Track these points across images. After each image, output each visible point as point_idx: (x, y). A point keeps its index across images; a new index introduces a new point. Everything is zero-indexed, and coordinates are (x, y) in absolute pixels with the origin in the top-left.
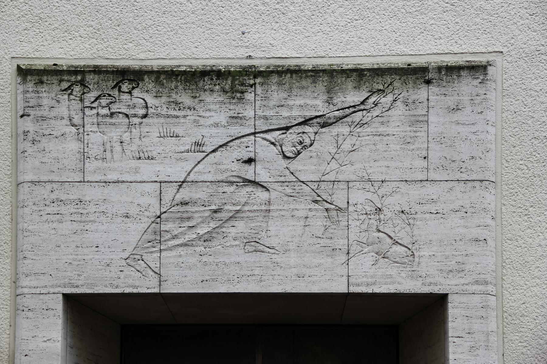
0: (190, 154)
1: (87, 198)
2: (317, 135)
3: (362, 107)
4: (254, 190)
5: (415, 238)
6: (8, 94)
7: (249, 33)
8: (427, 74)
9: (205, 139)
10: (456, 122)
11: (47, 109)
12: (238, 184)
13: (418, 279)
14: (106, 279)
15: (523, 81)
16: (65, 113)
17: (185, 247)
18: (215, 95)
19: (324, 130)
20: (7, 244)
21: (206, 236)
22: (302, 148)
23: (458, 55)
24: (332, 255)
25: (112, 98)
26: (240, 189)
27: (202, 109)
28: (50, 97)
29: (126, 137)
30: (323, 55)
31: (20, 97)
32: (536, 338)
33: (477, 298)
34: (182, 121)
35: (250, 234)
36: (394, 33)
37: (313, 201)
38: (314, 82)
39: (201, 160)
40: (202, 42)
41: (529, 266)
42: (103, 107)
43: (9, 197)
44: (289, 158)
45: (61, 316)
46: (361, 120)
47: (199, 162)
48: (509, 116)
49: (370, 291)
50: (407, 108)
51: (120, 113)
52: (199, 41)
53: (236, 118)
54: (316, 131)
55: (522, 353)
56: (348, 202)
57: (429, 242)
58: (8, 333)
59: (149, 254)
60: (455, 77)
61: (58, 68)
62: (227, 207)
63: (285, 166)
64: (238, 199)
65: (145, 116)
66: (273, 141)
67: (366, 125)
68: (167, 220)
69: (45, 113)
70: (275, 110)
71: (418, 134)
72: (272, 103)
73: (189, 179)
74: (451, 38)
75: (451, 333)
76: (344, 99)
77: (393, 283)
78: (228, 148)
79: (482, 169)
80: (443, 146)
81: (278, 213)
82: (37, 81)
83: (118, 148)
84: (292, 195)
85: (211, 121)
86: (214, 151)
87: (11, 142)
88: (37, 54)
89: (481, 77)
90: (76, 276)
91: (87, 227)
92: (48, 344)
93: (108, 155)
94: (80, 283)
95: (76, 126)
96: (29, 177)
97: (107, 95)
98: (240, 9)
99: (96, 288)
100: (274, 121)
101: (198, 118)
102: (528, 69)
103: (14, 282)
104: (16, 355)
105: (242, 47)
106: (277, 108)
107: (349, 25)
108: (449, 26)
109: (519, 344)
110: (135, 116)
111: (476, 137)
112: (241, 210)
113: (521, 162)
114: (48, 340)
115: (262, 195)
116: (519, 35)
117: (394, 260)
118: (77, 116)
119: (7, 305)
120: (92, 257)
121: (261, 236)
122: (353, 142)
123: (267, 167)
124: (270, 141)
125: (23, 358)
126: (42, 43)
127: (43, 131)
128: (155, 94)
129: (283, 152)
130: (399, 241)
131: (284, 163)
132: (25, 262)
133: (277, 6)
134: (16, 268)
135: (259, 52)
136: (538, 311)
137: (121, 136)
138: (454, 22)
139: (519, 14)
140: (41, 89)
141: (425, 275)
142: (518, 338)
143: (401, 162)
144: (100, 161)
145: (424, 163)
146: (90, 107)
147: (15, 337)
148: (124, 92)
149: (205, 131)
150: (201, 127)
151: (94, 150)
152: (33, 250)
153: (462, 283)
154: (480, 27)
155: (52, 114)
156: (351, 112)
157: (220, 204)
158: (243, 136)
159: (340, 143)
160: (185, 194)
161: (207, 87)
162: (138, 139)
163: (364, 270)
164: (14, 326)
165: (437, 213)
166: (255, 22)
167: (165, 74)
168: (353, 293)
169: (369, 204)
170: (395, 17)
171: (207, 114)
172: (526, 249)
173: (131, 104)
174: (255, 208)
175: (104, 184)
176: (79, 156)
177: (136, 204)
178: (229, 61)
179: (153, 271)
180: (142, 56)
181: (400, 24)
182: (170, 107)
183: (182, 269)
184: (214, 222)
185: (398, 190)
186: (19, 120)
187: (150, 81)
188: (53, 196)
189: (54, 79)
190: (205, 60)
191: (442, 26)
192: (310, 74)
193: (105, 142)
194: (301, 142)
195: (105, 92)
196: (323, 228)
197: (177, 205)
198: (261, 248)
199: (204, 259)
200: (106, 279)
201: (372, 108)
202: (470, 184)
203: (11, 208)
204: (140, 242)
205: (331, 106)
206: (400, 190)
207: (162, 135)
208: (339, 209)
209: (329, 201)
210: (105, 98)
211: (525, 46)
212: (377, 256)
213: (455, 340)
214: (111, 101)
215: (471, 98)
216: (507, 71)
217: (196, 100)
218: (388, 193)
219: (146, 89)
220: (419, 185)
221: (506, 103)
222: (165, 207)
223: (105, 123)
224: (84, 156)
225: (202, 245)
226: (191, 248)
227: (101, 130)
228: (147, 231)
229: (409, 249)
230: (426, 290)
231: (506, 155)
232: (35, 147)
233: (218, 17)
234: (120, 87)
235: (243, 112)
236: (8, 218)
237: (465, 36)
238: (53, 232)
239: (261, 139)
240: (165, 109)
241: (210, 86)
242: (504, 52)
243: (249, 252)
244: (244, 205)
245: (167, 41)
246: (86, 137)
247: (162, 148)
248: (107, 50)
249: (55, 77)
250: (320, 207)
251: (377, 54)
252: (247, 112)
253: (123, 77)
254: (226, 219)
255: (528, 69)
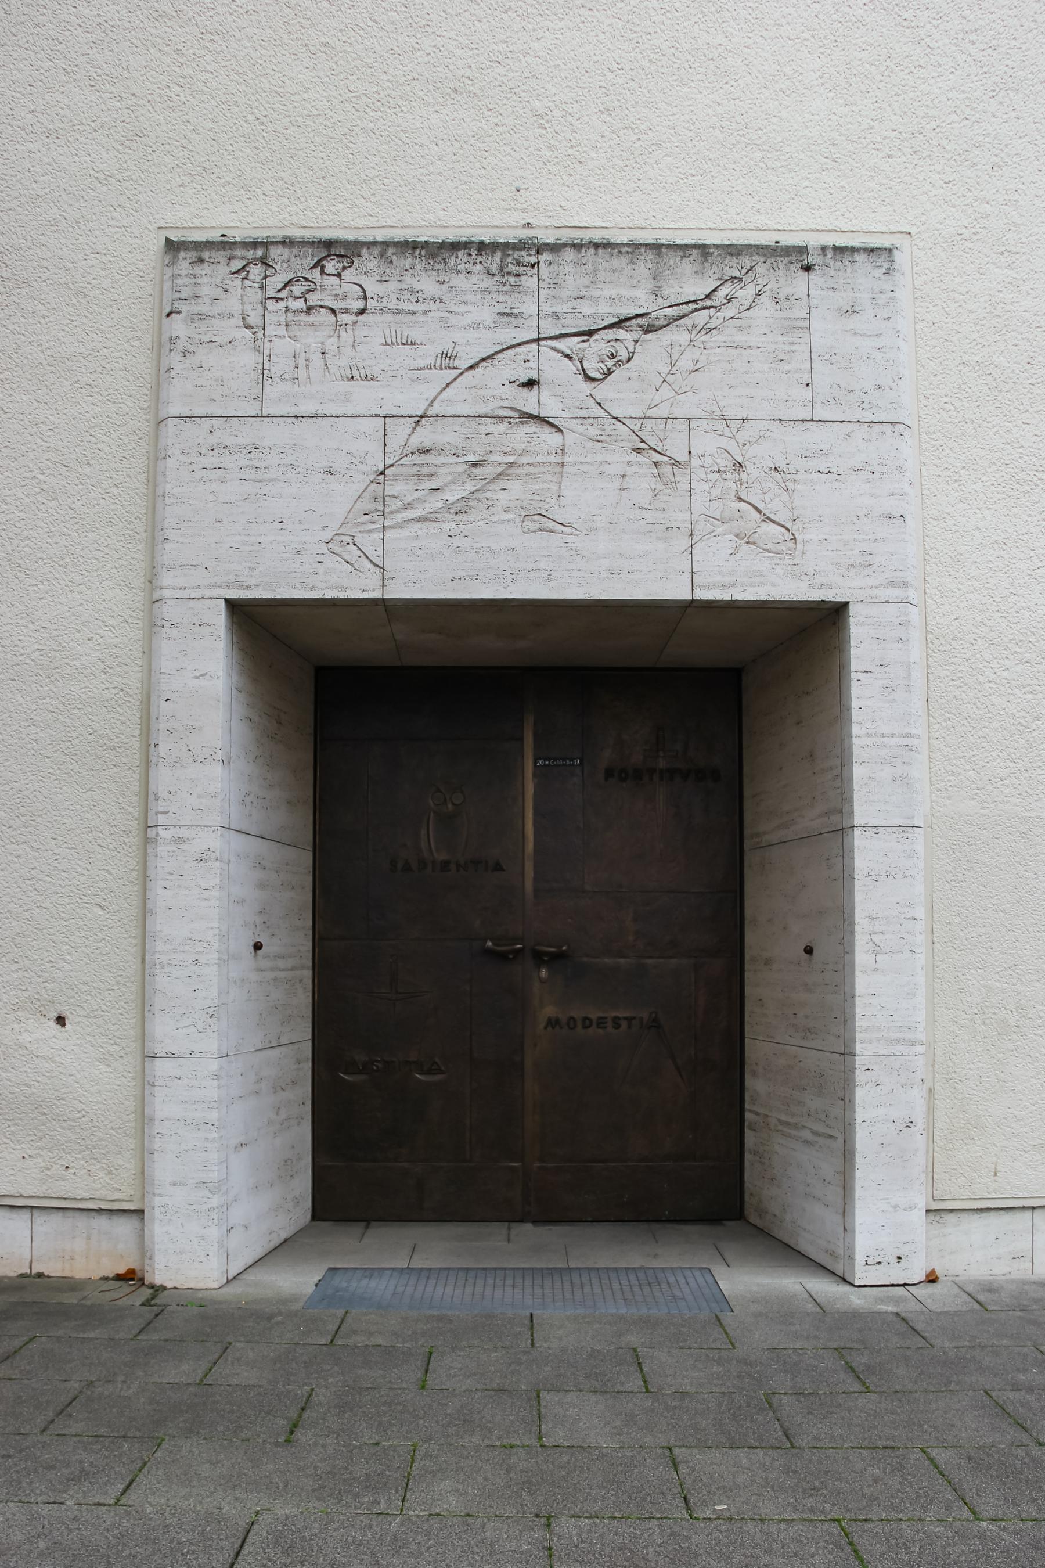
0: (434, 371)
1: (267, 443)
2: (638, 344)
3: (708, 303)
4: (537, 430)
5: (796, 512)
6: (149, 283)
7: (527, 189)
8: (805, 256)
9: (457, 348)
10: (853, 332)
11: (208, 301)
12: (512, 420)
13: (802, 578)
14: (295, 575)
15: (942, 278)
16: (236, 308)
17: (426, 523)
18: (475, 279)
19: (649, 336)
20: (140, 520)
21: (459, 504)
22: (614, 365)
23: (847, 234)
24: (666, 538)
25: (309, 283)
26: (514, 428)
27: (452, 301)
28: (213, 284)
29: (331, 344)
30: (644, 225)
31: (167, 285)
32: (975, 673)
33: (892, 609)
34: (422, 320)
35: (531, 502)
36: (750, 197)
37: (634, 450)
38: (632, 262)
39: (452, 382)
40: (453, 203)
41: (962, 561)
42: (296, 298)
43: (144, 444)
44: (593, 380)
45: (223, 636)
46: (708, 323)
47: (448, 385)
48: (926, 329)
49: (727, 598)
50: (778, 306)
51: (321, 307)
52: (449, 200)
53: (508, 315)
54: (636, 338)
55: (955, 697)
56: (690, 452)
57: (817, 518)
58: (140, 663)
59: (365, 535)
60: (847, 263)
61: (227, 239)
62: (493, 458)
63: (588, 393)
64: (511, 445)
65: (362, 312)
66: (568, 352)
67: (714, 331)
68: (395, 478)
69: (204, 309)
70: (570, 305)
71: (794, 348)
72: (565, 293)
73: (432, 411)
74: (835, 209)
75: (854, 665)
76: (680, 290)
77: (762, 584)
78: (495, 362)
79: (893, 405)
80: (834, 366)
81: (577, 467)
82: (194, 259)
83: (317, 362)
84: (599, 438)
85: (468, 320)
86: (471, 367)
87: (152, 358)
88: (197, 223)
89: (886, 265)
90: (247, 570)
91: (265, 490)
92: (202, 682)
93: (302, 373)
94: (252, 581)
95: (252, 328)
96: (174, 410)
97: (302, 279)
98: (513, 153)
99: (279, 590)
100: (569, 321)
101: (446, 315)
102: (948, 261)
103: (150, 582)
104: (152, 699)
105: (516, 210)
106: (573, 300)
107: (681, 181)
108: (832, 192)
109: (951, 683)
110: (346, 311)
111: (882, 355)
112: (516, 463)
113: (946, 399)
114: (202, 675)
115: (552, 439)
116: (932, 210)
117: (765, 547)
118: (254, 312)
119: (139, 619)
120: (273, 538)
121: (549, 505)
122: (696, 357)
123: (558, 393)
124: (562, 353)
125: (163, 704)
126: (205, 206)
127: (200, 336)
128: (379, 278)
129: (584, 370)
130: (772, 517)
131: (587, 387)
132: (166, 546)
133: (570, 151)
134: (153, 558)
135: (543, 219)
136: (977, 630)
137: (322, 343)
138: (838, 185)
139: (929, 180)
140: (200, 272)
141: (813, 572)
142: (948, 673)
143: (772, 390)
144: (289, 383)
145: (807, 393)
146: (275, 298)
147: (150, 670)
148: (328, 275)
149: (458, 336)
150: (451, 329)
151: (280, 366)
152: (179, 526)
153: (870, 584)
154: (876, 195)
155: (216, 310)
156: (690, 310)
157: (482, 453)
158: (519, 344)
159: (674, 358)
160: (424, 436)
161: (461, 267)
162: (350, 348)
163: (717, 563)
164: (149, 652)
165: (829, 472)
166: (536, 174)
167: (394, 246)
168: (701, 601)
169: (723, 456)
170: (750, 174)
171: (462, 308)
172: (958, 534)
173: (340, 292)
174: (539, 459)
175: (294, 420)
176: (256, 374)
177: (345, 451)
178: (496, 231)
179: (371, 562)
180: (359, 223)
181: (758, 184)
182: (403, 297)
183: (419, 559)
184: (472, 482)
185: (768, 434)
186: (165, 320)
187: (372, 257)
188: (213, 440)
189: (221, 256)
190: (457, 230)
191: (821, 191)
192: (625, 249)
193: (297, 352)
194: (612, 354)
195: (299, 275)
196: (651, 494)
197: (412, 453)
198: (550, 524)
199: (456, 542)
200: (295, 575)
201: (724, 305)
202: (877, 428)
203: (147, 462)
204: (351, 514)
205: (660, 299)
206: (771, 434)
207: (389, 341)
208: (676, 463)
209: (660, 450)
210: (299, 283)
211: (941, 226)
212: (737, 540)
213: (861, 676)
214: (308, 288)
215: (872, 296)
216: (919, 261)
217: (445, 287)
218: (753, 440)
219: (364, 270)
220: (800, 426)
221: (920, 309)
222: (392, 457)
223: (298, 323)
224: (263, 375)
225: (453, 520)
226: (434, 524)
227: (291, 334)
228: (363, 496)
229: (788, 530)
230: (815, 596)
231: (923, 388)
232: (187, 361)
233: (478, 165)
234: (323, 267)
235: (518, 305)
236: (142, 477)
237: (856, 207)
238: (211, 497)
239: (548, 350)
240: (395, 301)
241: (467, 266)
242: (912, 234)
243: (530, 532)
244: (521, 455)
245: (398, 200)
246: (267, 345)
247: (389, 362)
248: (304, 215)
249: (222, 253)
250: (645, 459)
251: (726, 227)
252: (526, 305)
253: (329, 251)
254: (492, 477)
255: (948, 261)
